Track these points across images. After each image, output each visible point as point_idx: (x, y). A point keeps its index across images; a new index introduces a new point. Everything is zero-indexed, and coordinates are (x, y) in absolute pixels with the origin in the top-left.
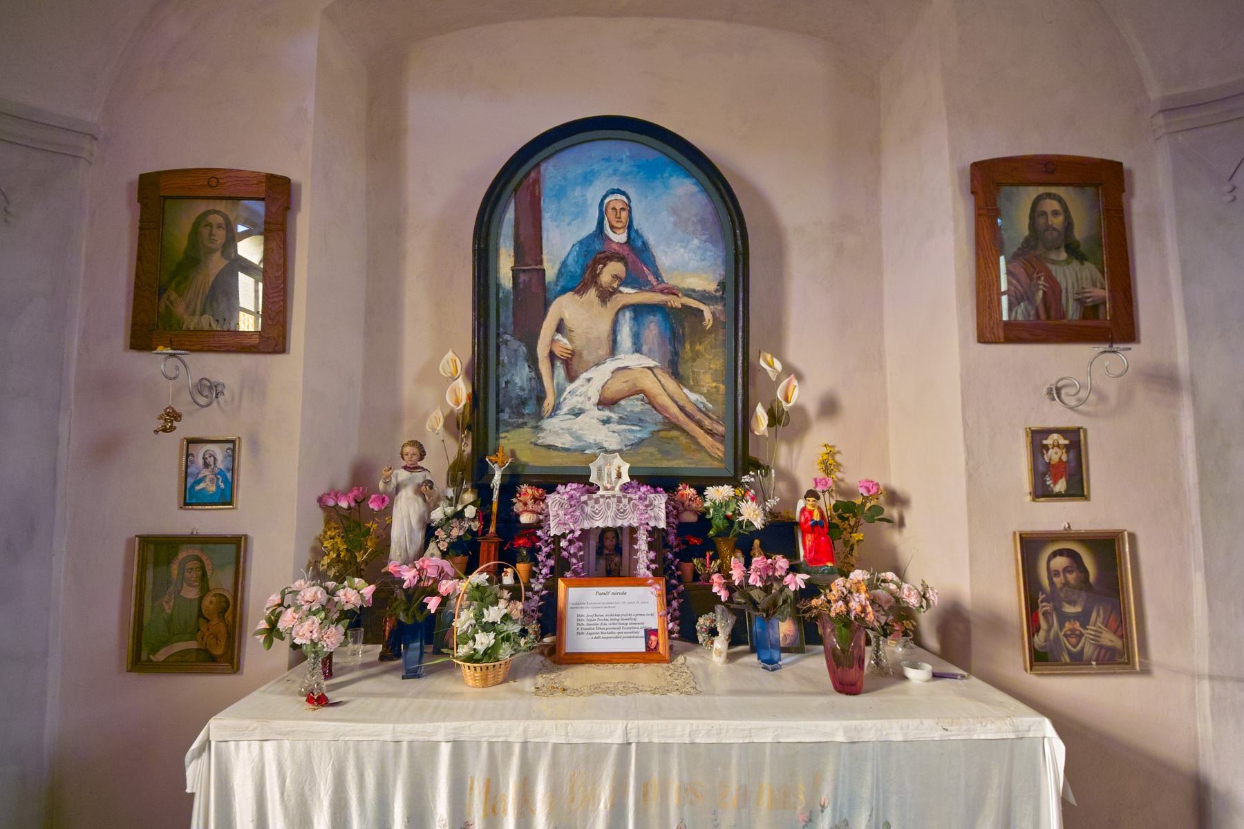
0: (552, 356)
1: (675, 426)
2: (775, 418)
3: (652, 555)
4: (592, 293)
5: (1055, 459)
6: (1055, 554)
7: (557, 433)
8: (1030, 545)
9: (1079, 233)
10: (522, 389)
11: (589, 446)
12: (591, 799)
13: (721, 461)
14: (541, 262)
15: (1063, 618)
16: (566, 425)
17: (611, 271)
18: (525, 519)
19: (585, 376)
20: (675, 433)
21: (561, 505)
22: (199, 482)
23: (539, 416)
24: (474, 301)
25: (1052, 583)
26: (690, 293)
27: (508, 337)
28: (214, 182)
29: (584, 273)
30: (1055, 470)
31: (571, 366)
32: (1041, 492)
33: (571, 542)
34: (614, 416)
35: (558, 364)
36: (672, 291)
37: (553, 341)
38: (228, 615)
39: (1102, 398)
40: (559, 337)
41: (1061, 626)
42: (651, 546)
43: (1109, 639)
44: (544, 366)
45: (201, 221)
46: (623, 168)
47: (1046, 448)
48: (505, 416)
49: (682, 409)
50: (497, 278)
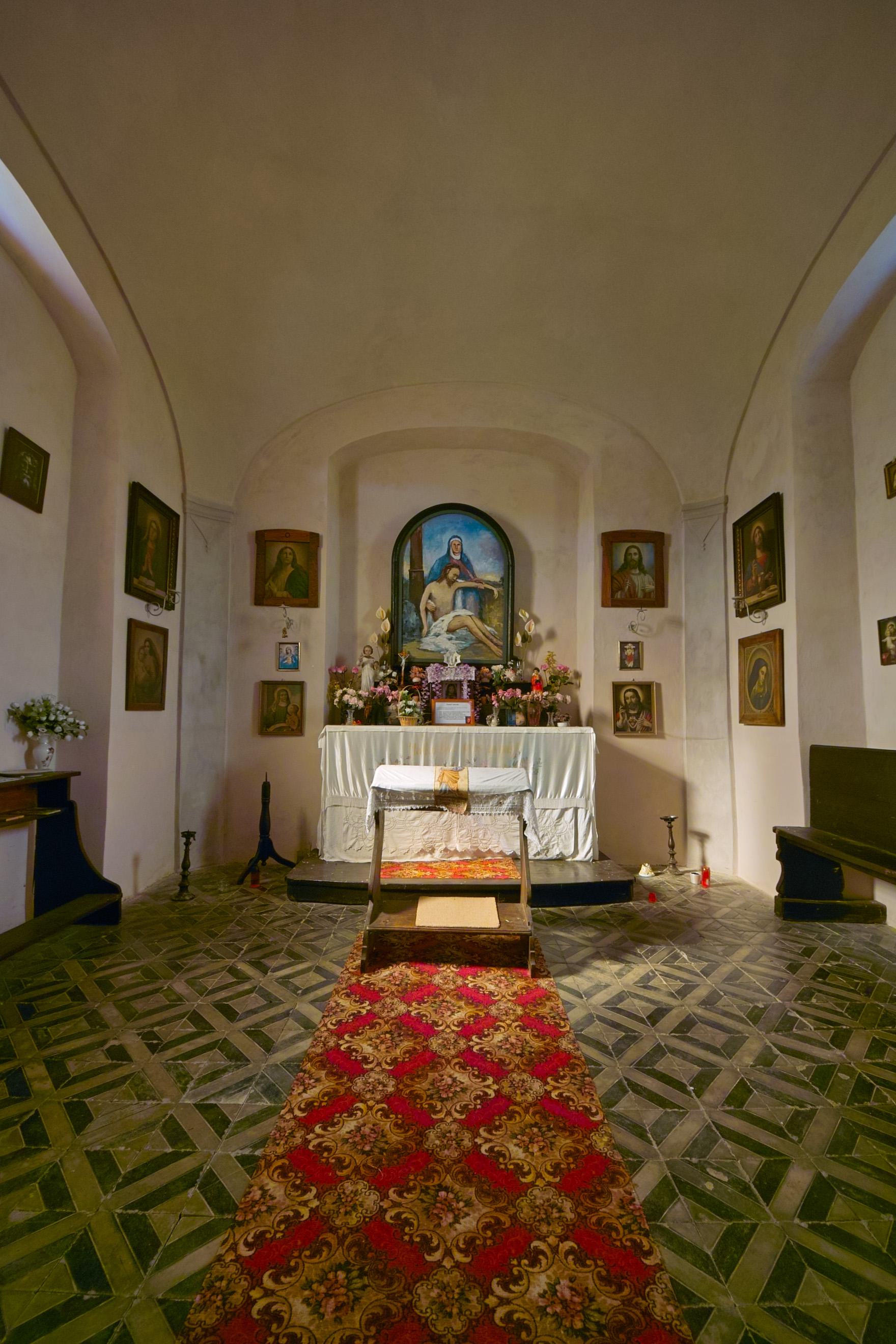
0: (427, 610)
1: (481, 642)
2: (525, 639)
3: (469, 690)
4: (444, 582)
5: (629, 654)
6: (627, 691)
7: (428, 644)
8: (617, 688)
9: (645, 562)
10: (413, 624)
11: (443, 650)
12: (448, 749)
13: (501, 657)
14: (422, 568)
15: (629, 715)
16: (432, 640)
17: (452, 573)
18: (415, 680)
19: (441, 619)
20: (480, 645)
21: (433, 671)
22: (284, 660)
23: (421, 636)
24: (803, 775)
25: (625, 702)
26: (488, 582)
27: (407, 601)
28: (288, 535)
29: (441, 573)
30: (630, 658)
31: (435, 614)
32: (623, 667)
33: (436, 685)
34: (454, 637)
35: (429, 613)
36: (480, 582)
37: (427, 603)
38: (299, 713)
39: (650, 629)
40: (430, 601)
41: (628, 718)
42: (469, 686)
43: (646, 723)
44: (423, 614)
45: (281, 551)
46: (459, 526)
47: (626, 649)
48: (405, 636)
49: (484, 634)
50: (402, 575)
